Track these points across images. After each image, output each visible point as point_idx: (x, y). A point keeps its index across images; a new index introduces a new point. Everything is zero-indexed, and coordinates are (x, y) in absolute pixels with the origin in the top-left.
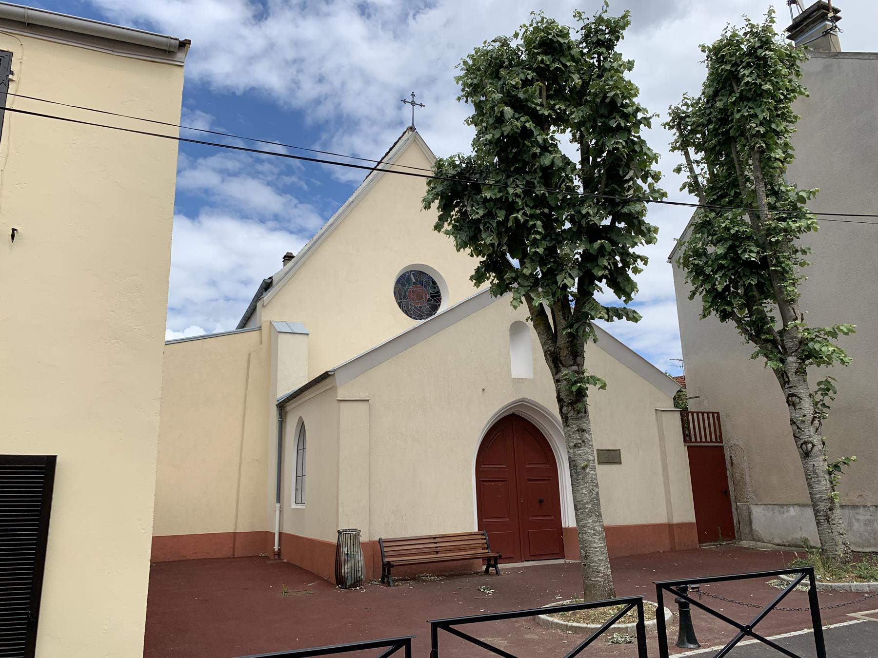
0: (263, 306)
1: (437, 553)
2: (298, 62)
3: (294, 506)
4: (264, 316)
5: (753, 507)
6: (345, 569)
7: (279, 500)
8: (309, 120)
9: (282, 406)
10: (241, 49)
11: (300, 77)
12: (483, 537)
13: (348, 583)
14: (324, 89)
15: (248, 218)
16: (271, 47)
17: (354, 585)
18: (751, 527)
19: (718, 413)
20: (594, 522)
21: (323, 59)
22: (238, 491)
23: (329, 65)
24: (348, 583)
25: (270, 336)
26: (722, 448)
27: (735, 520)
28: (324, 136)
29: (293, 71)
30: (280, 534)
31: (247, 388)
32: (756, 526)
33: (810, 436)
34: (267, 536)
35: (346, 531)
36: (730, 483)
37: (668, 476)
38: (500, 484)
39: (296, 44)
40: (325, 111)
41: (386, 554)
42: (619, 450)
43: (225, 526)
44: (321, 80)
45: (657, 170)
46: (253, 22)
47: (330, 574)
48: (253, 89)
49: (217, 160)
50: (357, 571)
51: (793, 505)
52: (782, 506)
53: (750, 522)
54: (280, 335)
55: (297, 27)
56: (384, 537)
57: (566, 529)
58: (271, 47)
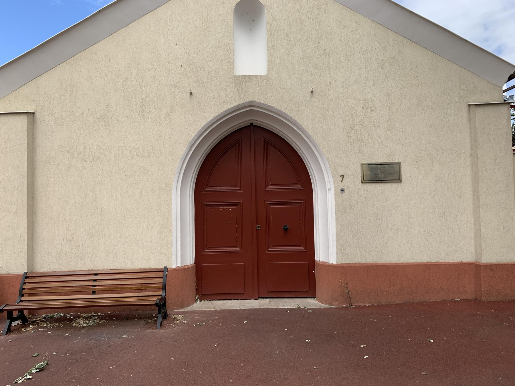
1: (94, 293)
42: (399, 164)
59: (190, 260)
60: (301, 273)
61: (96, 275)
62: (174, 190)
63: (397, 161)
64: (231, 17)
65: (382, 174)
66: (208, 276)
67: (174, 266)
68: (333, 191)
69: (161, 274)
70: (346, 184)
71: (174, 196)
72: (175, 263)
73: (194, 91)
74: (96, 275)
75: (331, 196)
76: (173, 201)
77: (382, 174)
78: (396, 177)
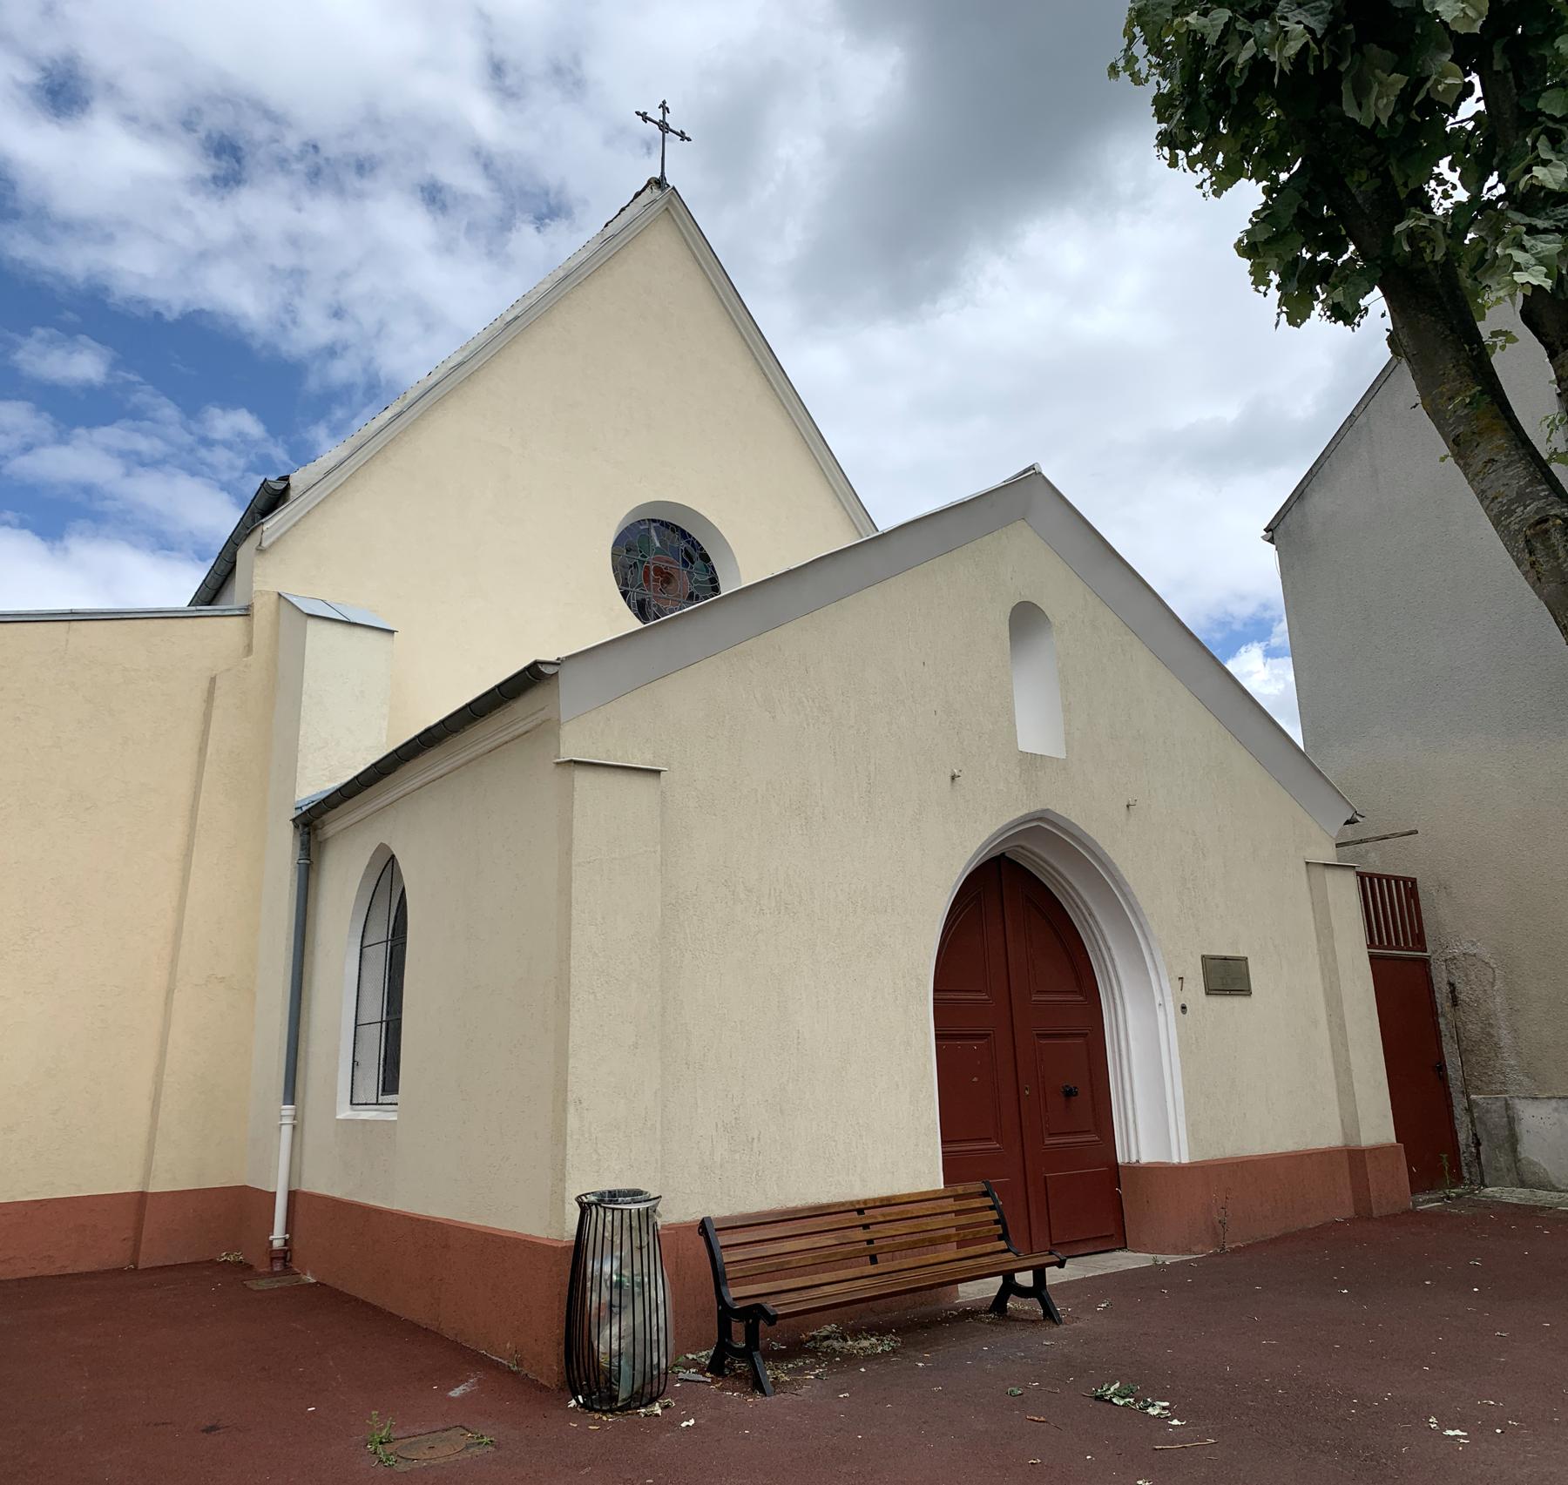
0: (261, 550)
2: (297, 275)
3: (345, 1112)
4: (261, 577)
6: (609, 1339)
7: (290, 1095)
8: (313, 384)
9: (312, 824)
10: (180, 234)
11: (297, 301)
12: (988, 1201)
13: (623, 1395)
14: (346, 330)
15: (172, 549)
16: (246, 241)
17: (644, 1397)
18: (1514, 1150)
21: (343, 276)
22: (162, 1054)
23: (358, 287)
24: (623, 1395)
25: (276, 623)
26: (1425, 962)
27: (1463, 1137)
28: (339, 413)
30: (292, 1196)
31: (202, 750)
32: (1531, 1149)
34: (245, 1204)
35: (613, 1196)
36: (1449, 1048)
37: (1342, 1027)
38: (975, 1045)
39: (294, 241)
40: (341, 371)
41: (731, 1271)
43: (116, 1177)
44: (338, 313)
47: (549, 1364)
48: (200, 312)
49: (113, 435)
50: (649, 1344)
53: (1513, 1140)
54: (311, 623)
55: (299, 210)
56: (718, 1209)
57: (1137, 1170)
58: (246, 241)
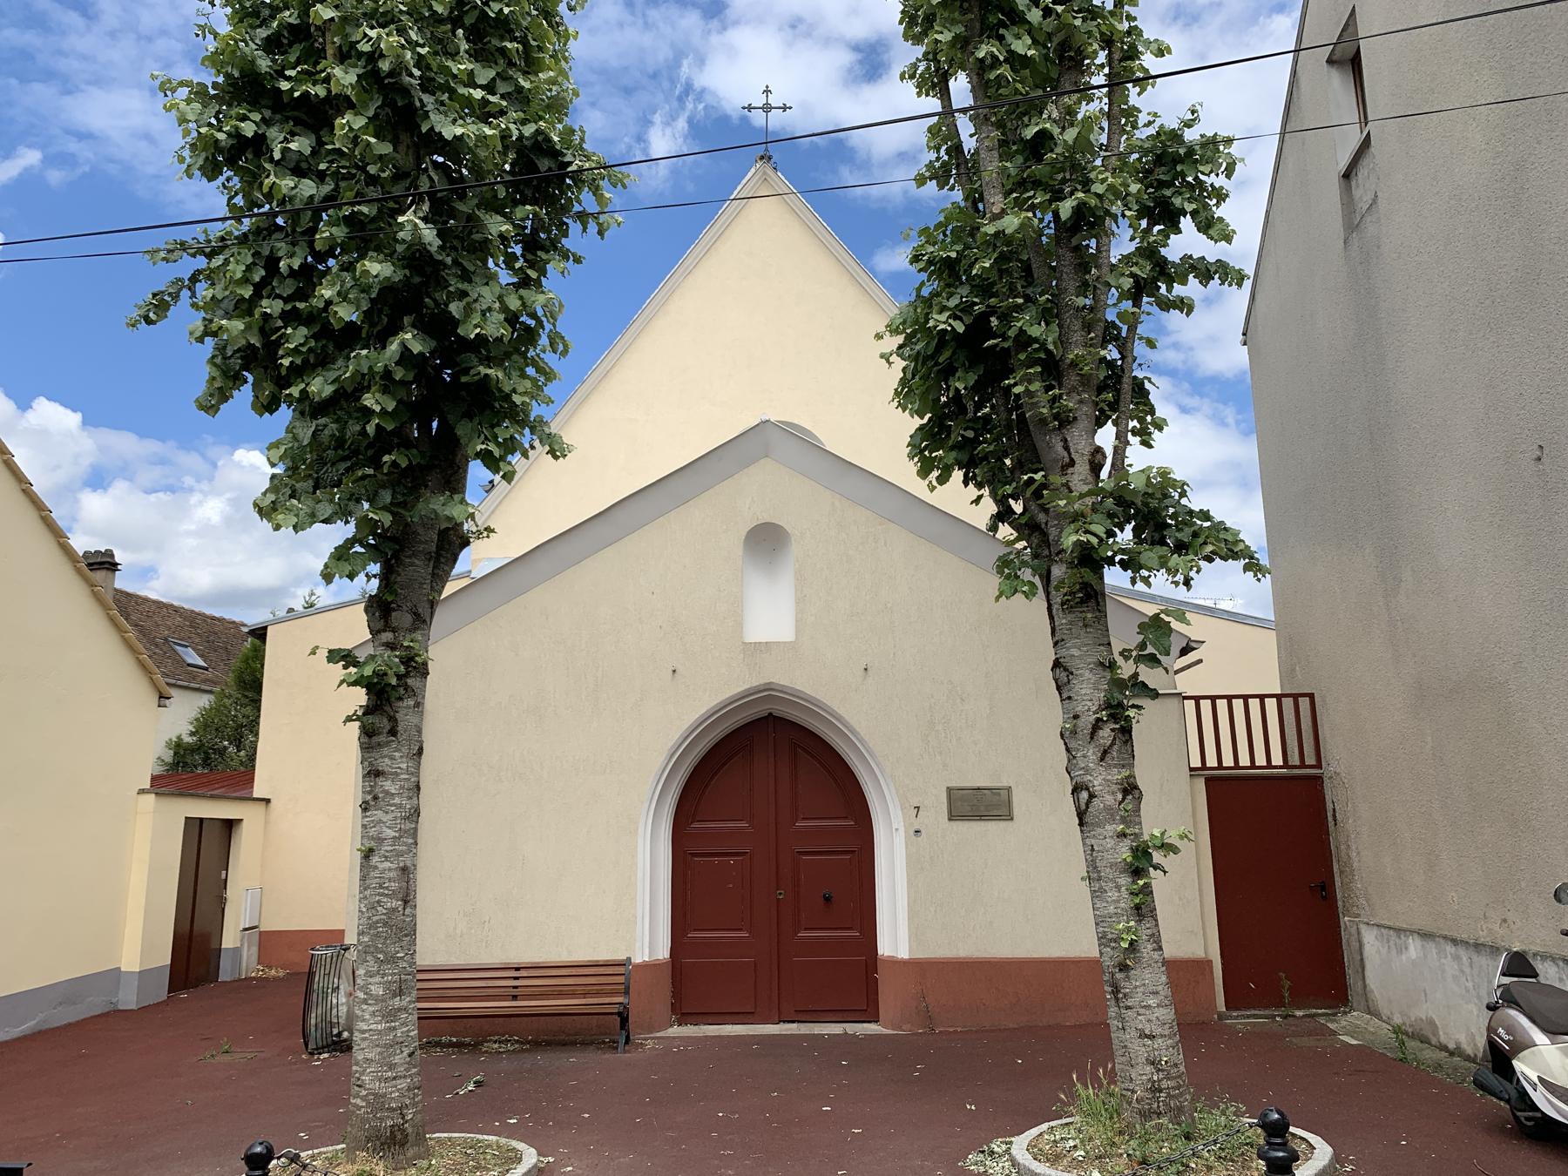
1: (515, 998)
5: (1363, 928)
19: (1311, 696)
20: (369, 974)
26: (1318, 780)
29: (174, 112)
33: (1087, 771)
42: (1009, 789)
45: (200, 184)
46: (715, 24)
51: (1412, 932)
52: (1398, 930)
59: (663, 952)
60: (854, 977)
61: (517, 969)
62: (641, 830)
63: (1005, 784)
64: (739, 550)
65: (978, 805)
66: (692, 980)
67: (637, 960)
68: (902, 830)
69: (621, 970)
70: (924, 821)
71: (640, 841)
72: (640, 957)
73: (680, 669)
74: (517, 969)
75: (900, 840)
76: (640, 849)
77: (978, 805)
78: (1004, 811)
